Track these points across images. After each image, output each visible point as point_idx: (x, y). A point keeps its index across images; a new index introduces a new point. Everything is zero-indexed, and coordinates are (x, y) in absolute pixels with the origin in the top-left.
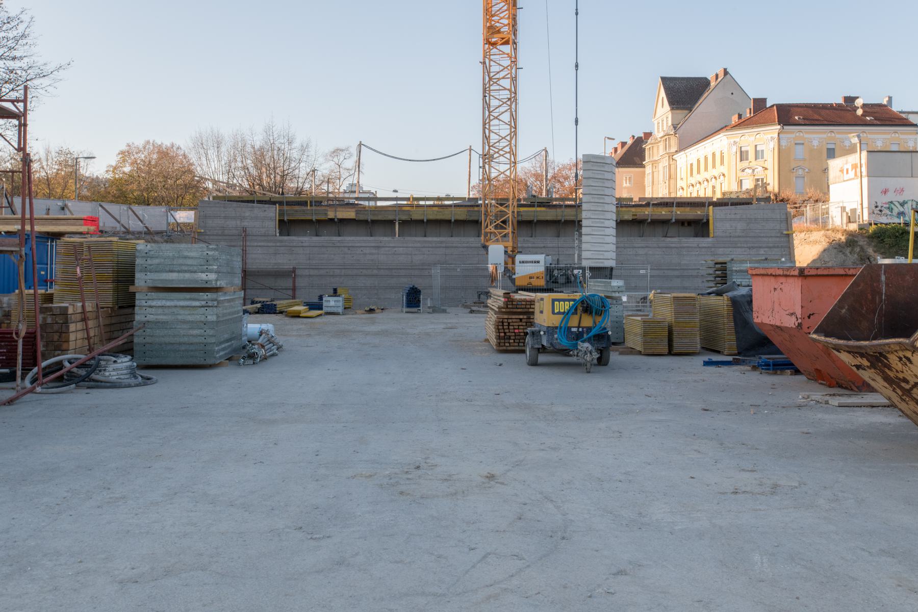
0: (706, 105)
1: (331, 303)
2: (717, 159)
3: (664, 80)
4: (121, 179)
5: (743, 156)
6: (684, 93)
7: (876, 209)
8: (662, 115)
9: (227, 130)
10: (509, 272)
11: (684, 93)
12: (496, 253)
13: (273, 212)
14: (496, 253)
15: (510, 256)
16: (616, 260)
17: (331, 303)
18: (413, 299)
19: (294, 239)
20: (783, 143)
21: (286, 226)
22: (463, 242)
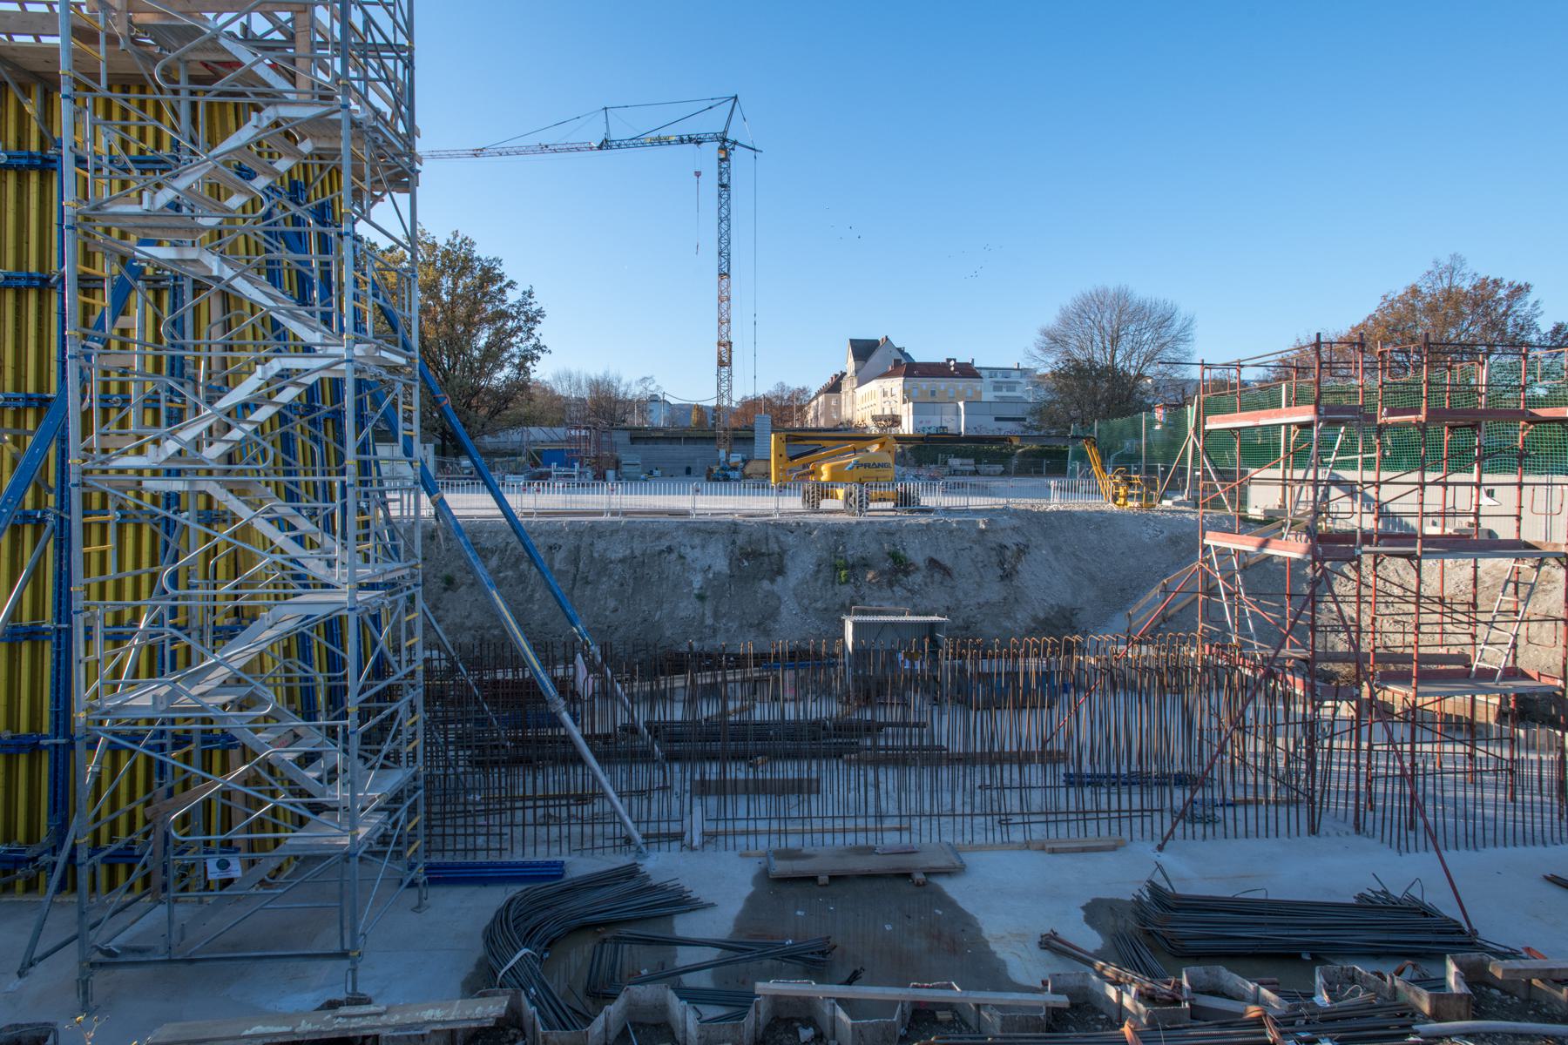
0: (875, 359)
1: (656, 473)
2: (873, 394)
3: (852, 341)
4: (1126, 375)
5: (885, 394)
6: (863, 350)
7: (915, 429)
8: (850, 365)
9: (574, 369)
10: (727, 461)
11: (863, 350)
12: (722, 453)
13: (627, 434)
14: (722, 453)
15: (728, 454)
16: (797, 722)
17: (656, 473)
18: (688, 471)
19: (636, 446)
20: (1014, 373)
21: (633, 440)
22: (711, 447)
